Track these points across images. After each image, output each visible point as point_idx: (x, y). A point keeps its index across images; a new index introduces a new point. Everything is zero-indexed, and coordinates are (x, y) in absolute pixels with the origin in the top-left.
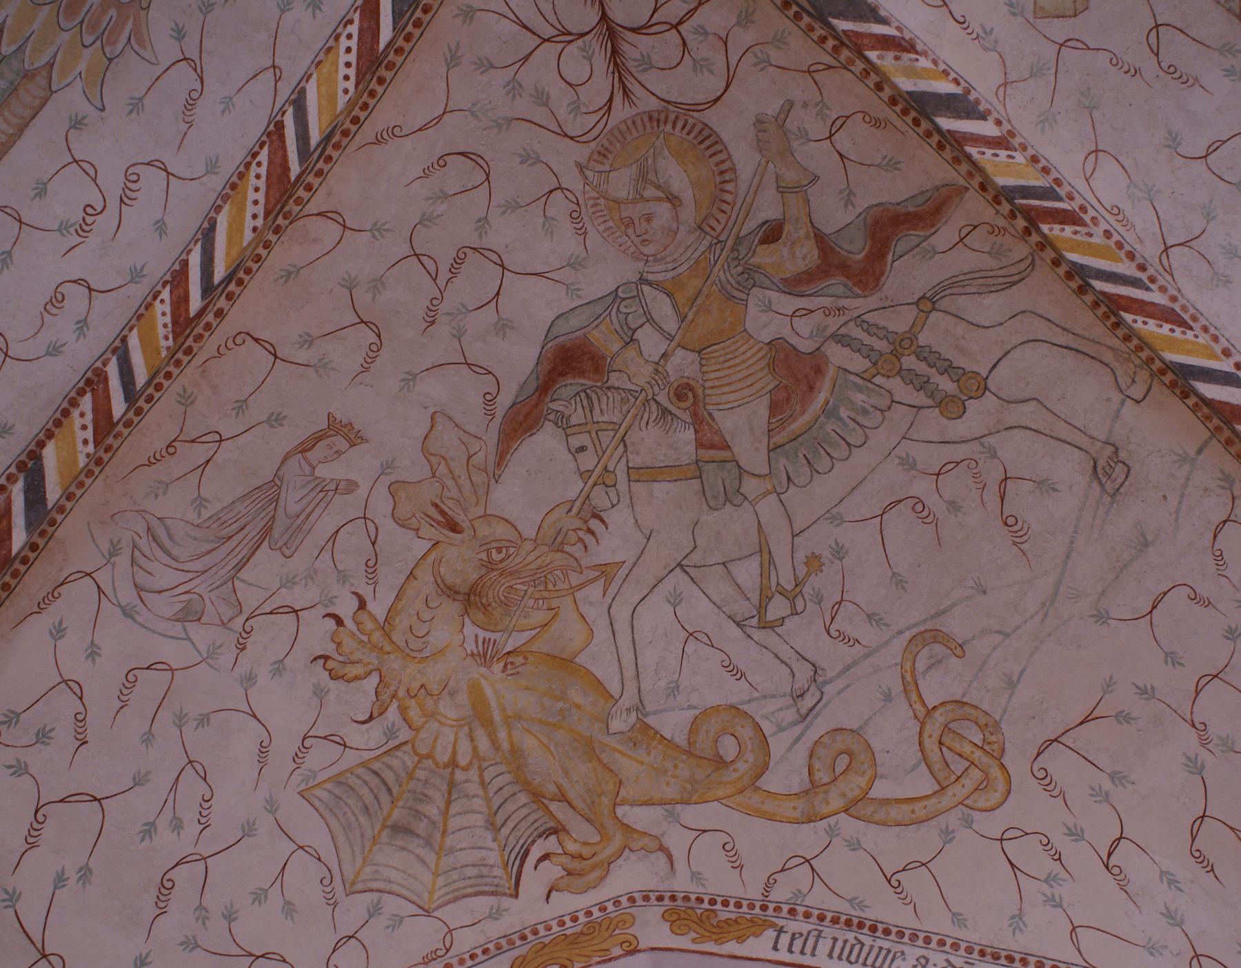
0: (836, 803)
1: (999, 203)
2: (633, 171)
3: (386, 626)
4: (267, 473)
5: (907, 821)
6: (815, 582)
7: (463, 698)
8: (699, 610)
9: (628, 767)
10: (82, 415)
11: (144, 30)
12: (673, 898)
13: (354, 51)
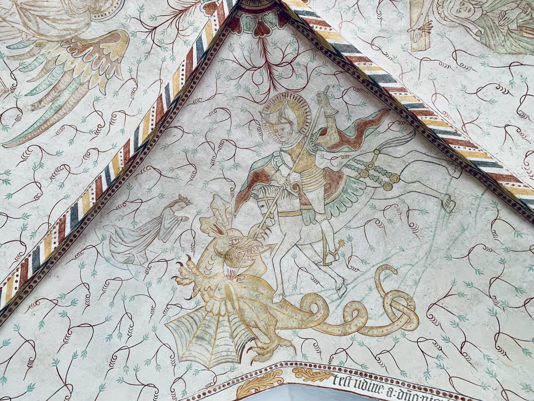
0: (354, 328)
1: (402, 113)
2: (277, 114)
3: (198, 266)
4: (158, 214)
5: (380, 335)
6: (342, 249)
7: (223, 291)
8: (302, 260)
9: (280, 316)
10: (92, 190)
11: (119, 70)
12: (296, 364)
13: (185, 70)
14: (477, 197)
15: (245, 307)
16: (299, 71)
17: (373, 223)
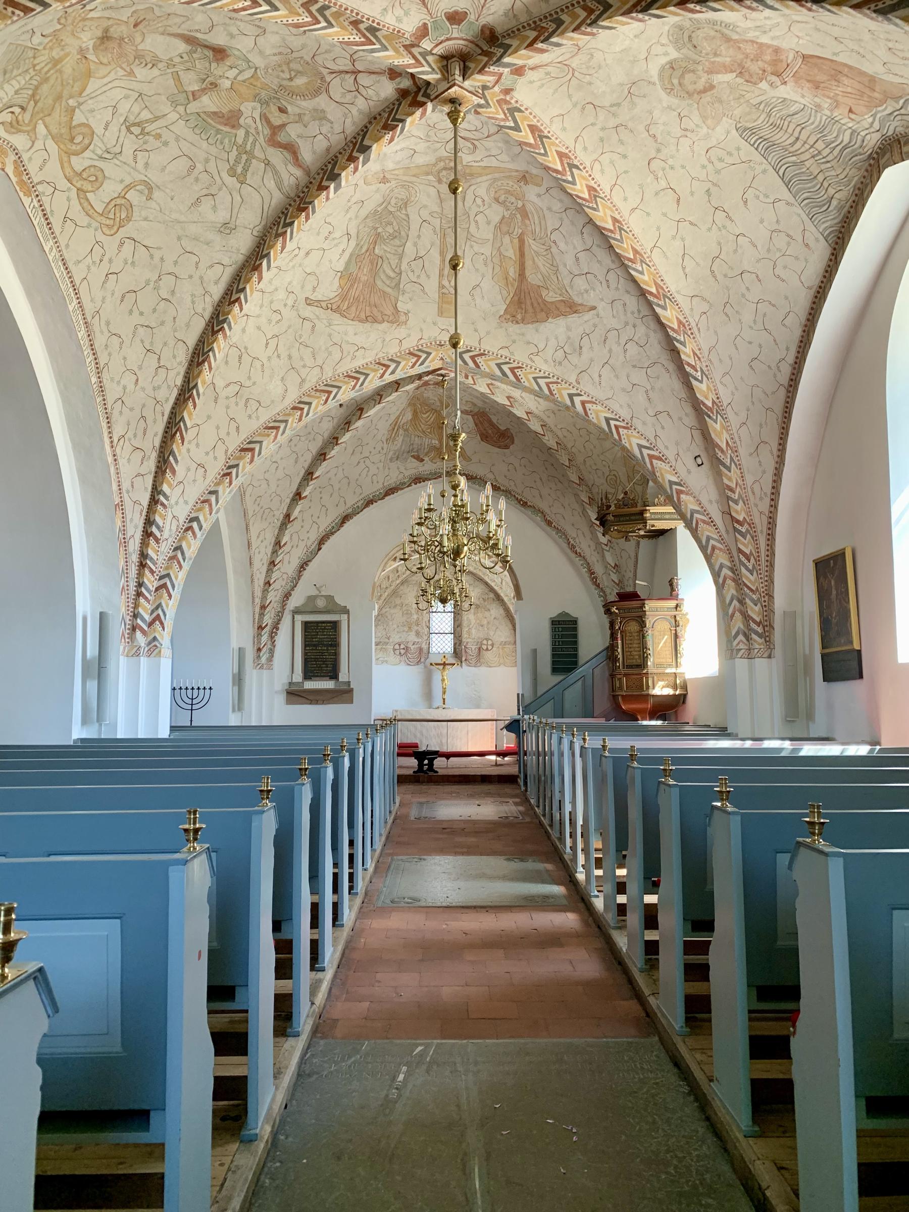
0: (78, 185)
2: (301, 69)
3: (84, 20)
7: (62, 53)
8: (124, 107)
9: (56, 114)
14: (238, 250)
15: (52, 81)
16: (349, 97)
17: (190, 163)
